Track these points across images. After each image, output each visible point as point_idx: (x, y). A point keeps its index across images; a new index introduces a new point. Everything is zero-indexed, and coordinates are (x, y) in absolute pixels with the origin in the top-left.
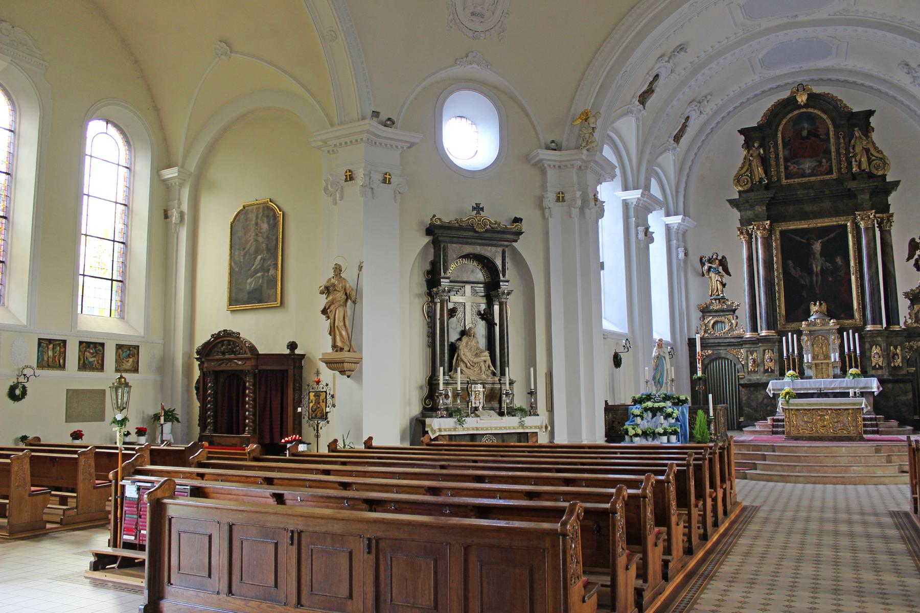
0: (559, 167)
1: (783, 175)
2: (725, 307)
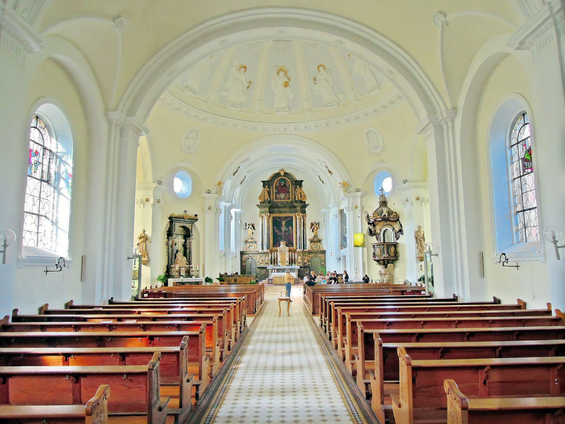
0: (210, 198)
1: (275, 198)
2: (253, 241)
